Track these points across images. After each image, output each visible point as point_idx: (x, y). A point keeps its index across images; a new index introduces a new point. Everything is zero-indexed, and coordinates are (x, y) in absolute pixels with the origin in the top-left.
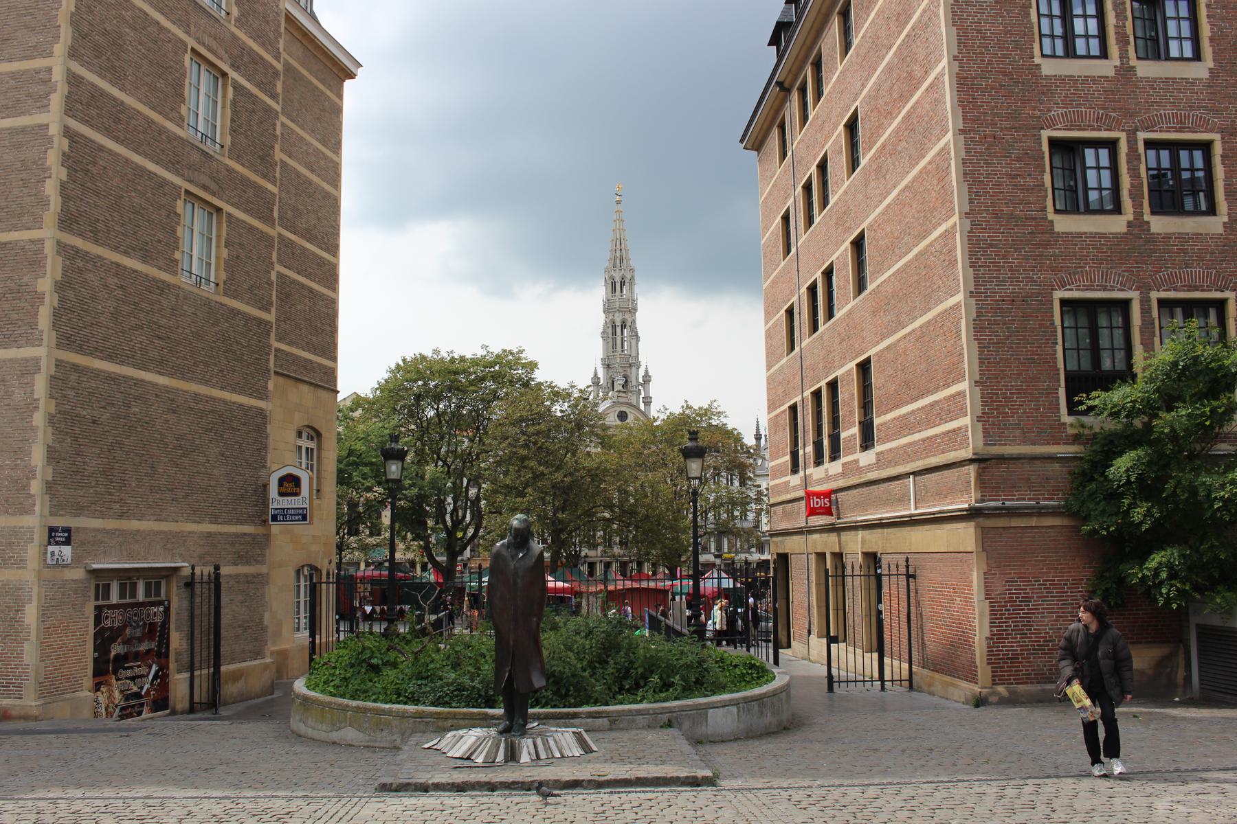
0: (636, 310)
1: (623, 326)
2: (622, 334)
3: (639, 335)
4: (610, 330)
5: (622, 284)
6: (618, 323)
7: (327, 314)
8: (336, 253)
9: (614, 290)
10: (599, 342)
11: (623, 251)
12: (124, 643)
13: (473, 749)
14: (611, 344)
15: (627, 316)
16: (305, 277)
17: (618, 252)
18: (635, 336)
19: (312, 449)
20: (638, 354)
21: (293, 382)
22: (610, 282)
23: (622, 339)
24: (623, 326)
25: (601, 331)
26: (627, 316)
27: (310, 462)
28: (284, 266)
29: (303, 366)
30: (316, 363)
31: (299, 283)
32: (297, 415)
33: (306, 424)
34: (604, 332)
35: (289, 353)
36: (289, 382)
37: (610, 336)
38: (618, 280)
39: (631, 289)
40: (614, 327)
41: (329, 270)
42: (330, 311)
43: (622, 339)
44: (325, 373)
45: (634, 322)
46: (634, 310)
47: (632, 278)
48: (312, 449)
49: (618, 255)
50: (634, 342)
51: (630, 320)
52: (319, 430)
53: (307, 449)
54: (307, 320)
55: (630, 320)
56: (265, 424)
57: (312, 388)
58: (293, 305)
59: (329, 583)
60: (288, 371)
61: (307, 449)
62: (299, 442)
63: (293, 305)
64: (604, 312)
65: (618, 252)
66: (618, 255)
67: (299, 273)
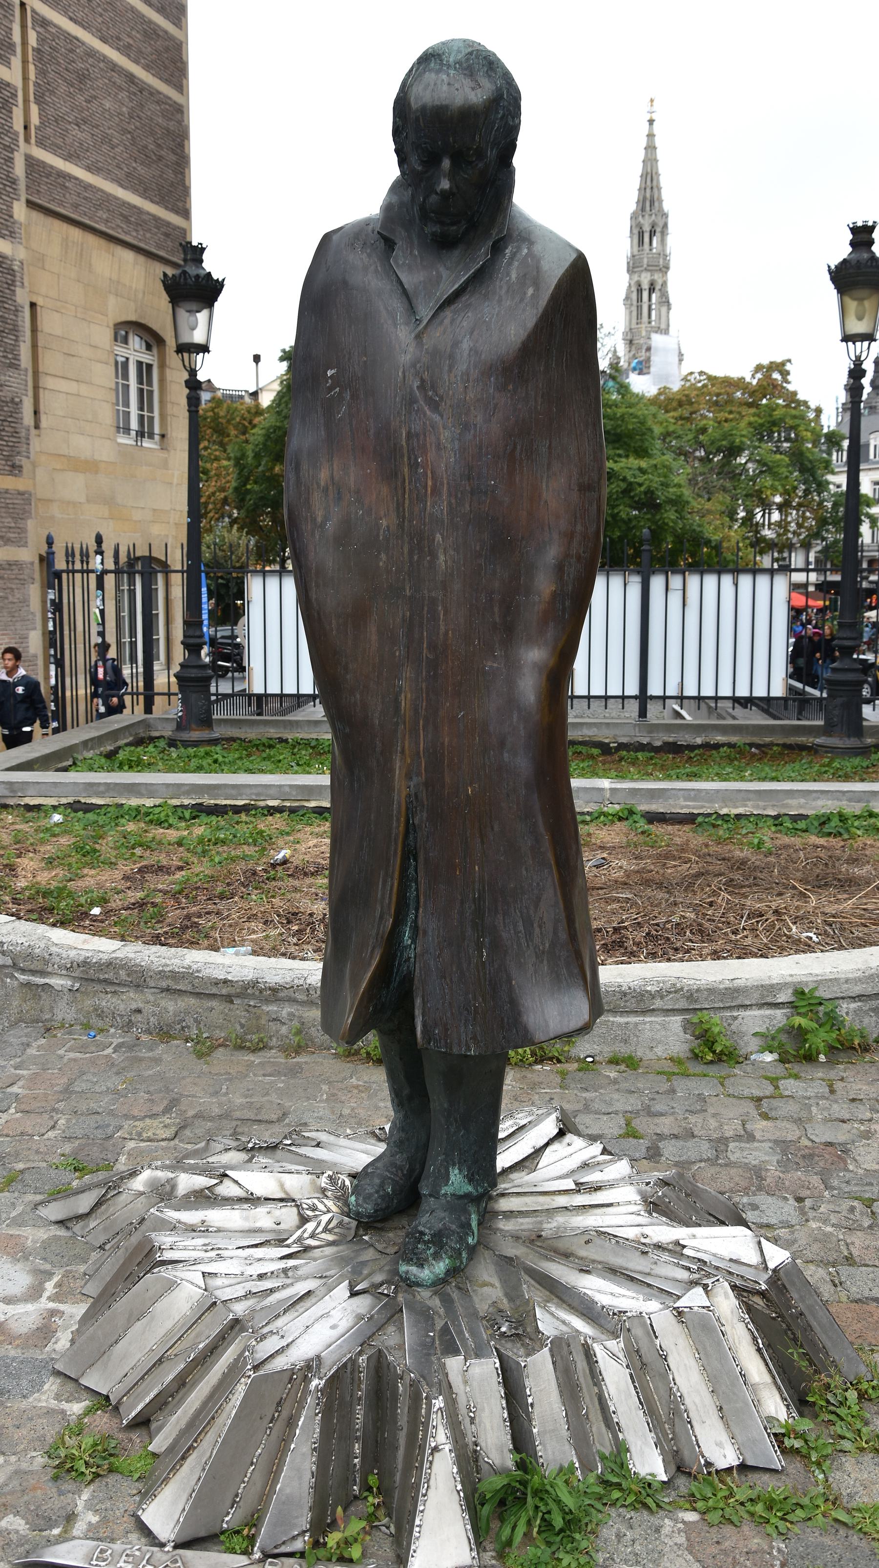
0: (667, 268)
1: (652, 290)
2: (650, 299)
3: (671, 301)
4: (634, 296)
5: (652, 233)
6: (645, 286)
7: (168, 130)
8: (179, 20)
9: (641, 242)
10: (661, 171)
11: (655, 190)
12: (395, 325)
13: (169, 1375)
14: (634, 314)
15: (657, 277)
16: (118, 49)
17: (648, 191)
18: (665, 302)
19: (149, 367)
20: (668, 325)
21: (102, 242)
22: (636, 231)
23: (650, 307)
24: (652, 290)
25: (624, 296)
26: (657, 277)
27: (145, 387)
28: (71, 19)
29: (122, 215)
30: (148, 213)
31: (105, 59)
32: (112, 301)
33: (133, 318)
34: (627, 298)
35: (90, 185)
36: (92, 240)
37: (635, 303)
38: (647, 228)
39: (663, 241)
40: (640, 291)
41: (167, 49)
42: (172, 125)
43: (650, 307)
44: (167, 235)
45: (664, 284)
46: (665, 268)
47: (665, 226)
48: (149, 367)
49: (648, 195)
50: (664, 310)
51: (660, 282)
52: (159, 331)
53: (140, 364)
54: (125, 131)
55: (660, 282)
56: (13, 283)
57: (141, 259)
58: (95, 97)
59: (74, 572)
60: (90, 218)
61: (140, 364)
62: (121, 351)
63: (95, 97)
64: (628, 271)
65: (648, 191)
66: (648, 195)
67: (104, 40)
